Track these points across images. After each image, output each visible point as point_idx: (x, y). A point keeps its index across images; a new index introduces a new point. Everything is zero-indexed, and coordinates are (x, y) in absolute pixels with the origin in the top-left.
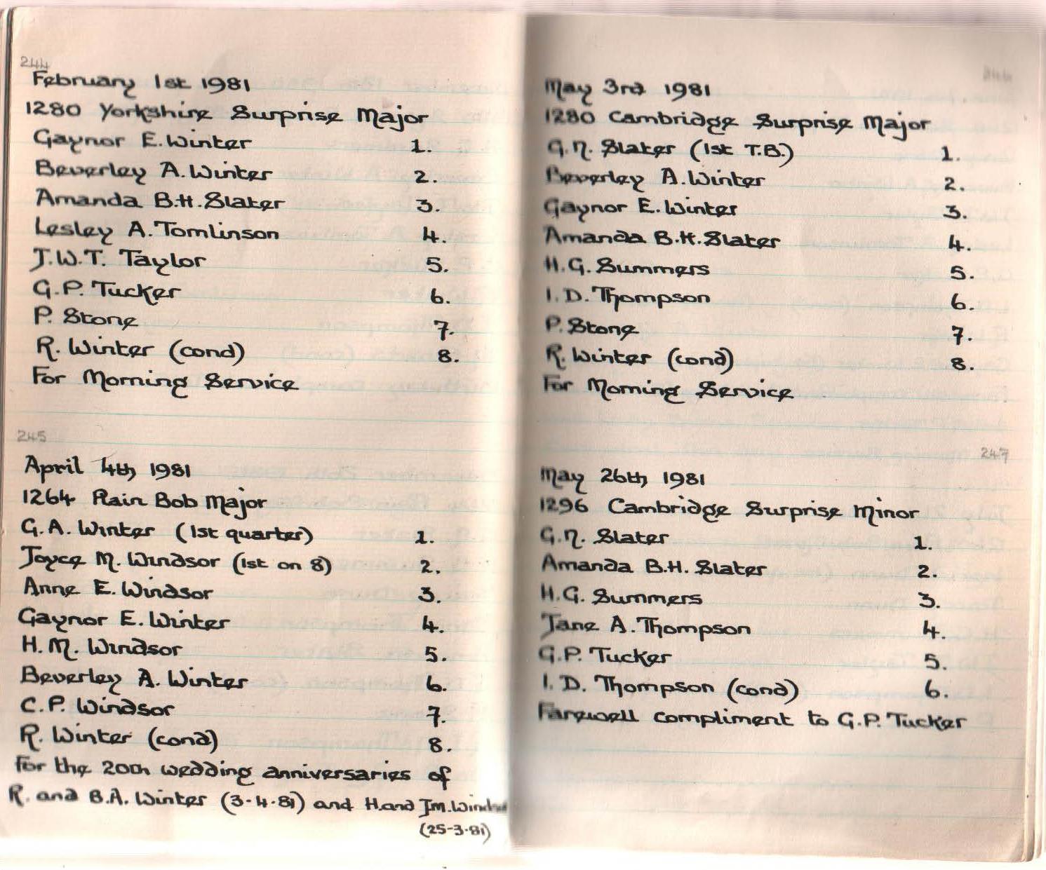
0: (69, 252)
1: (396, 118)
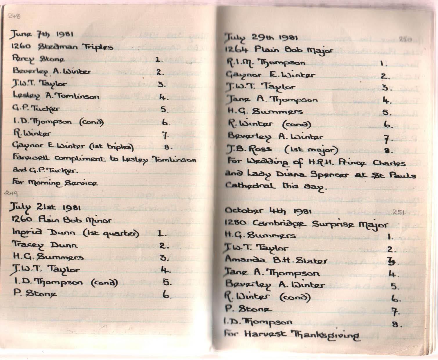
1: (322, 51)
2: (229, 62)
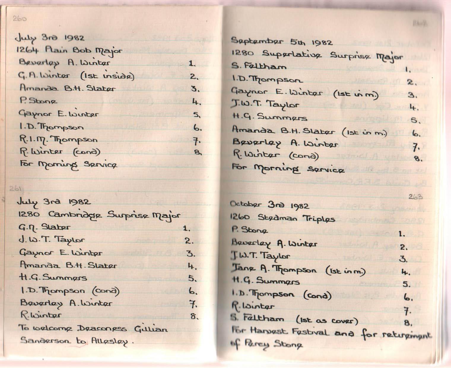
2: (234, 307)
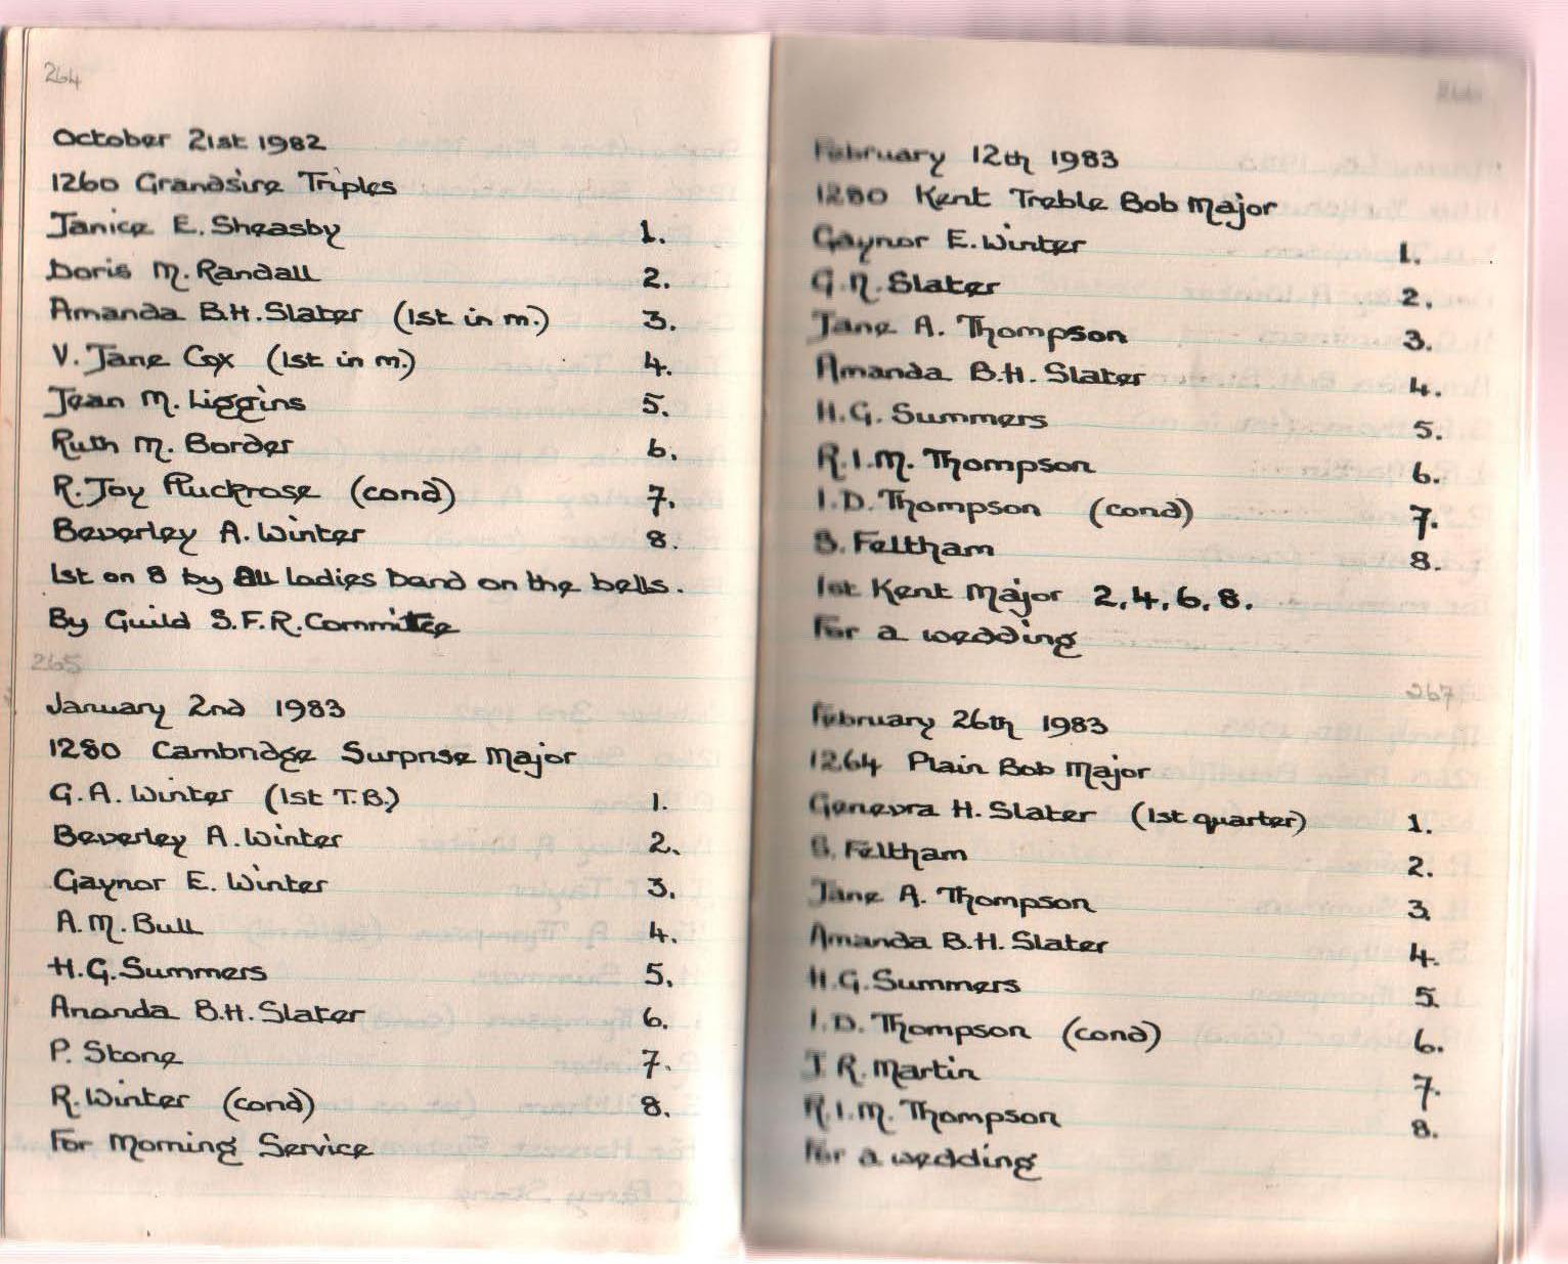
0: (244, 876)
